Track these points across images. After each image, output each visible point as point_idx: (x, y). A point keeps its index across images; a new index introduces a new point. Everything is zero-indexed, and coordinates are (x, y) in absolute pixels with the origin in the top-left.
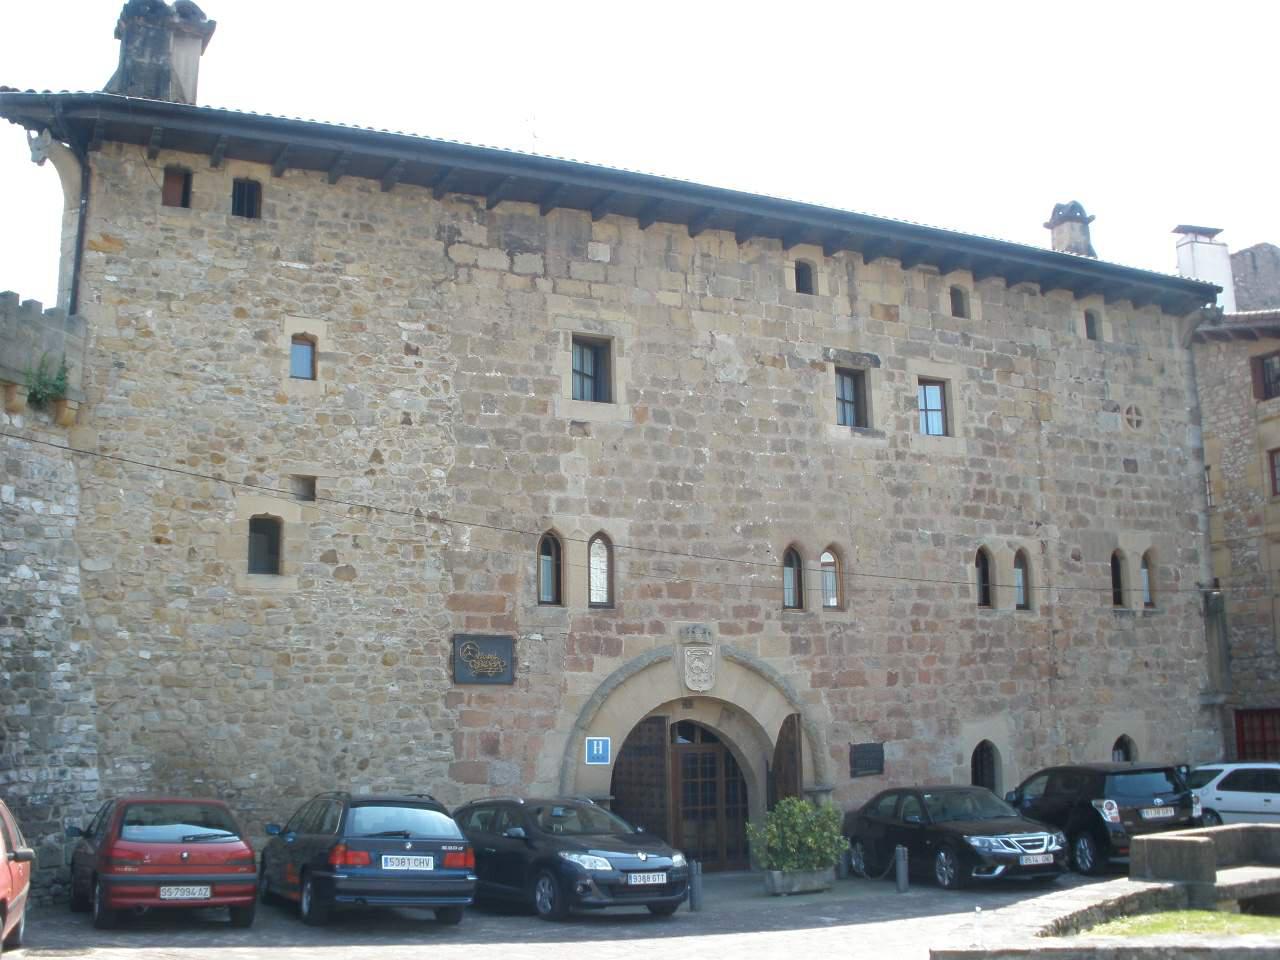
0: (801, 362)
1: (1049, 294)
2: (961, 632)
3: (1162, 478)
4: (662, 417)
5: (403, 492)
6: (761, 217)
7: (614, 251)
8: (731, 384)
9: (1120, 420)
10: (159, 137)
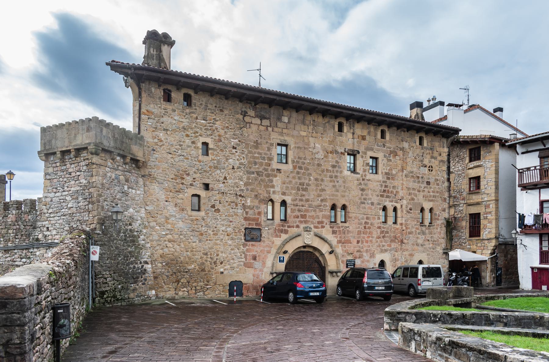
0: (338, 153)
1: (409, 132)
2: (377, 229)
3: (437, 187)
4: (300, 168)
5: (232, 189)
6: (330, 110)
7: (289, 119)
8: (319, 159)
9: (426, 170)
10: (162, 80)
